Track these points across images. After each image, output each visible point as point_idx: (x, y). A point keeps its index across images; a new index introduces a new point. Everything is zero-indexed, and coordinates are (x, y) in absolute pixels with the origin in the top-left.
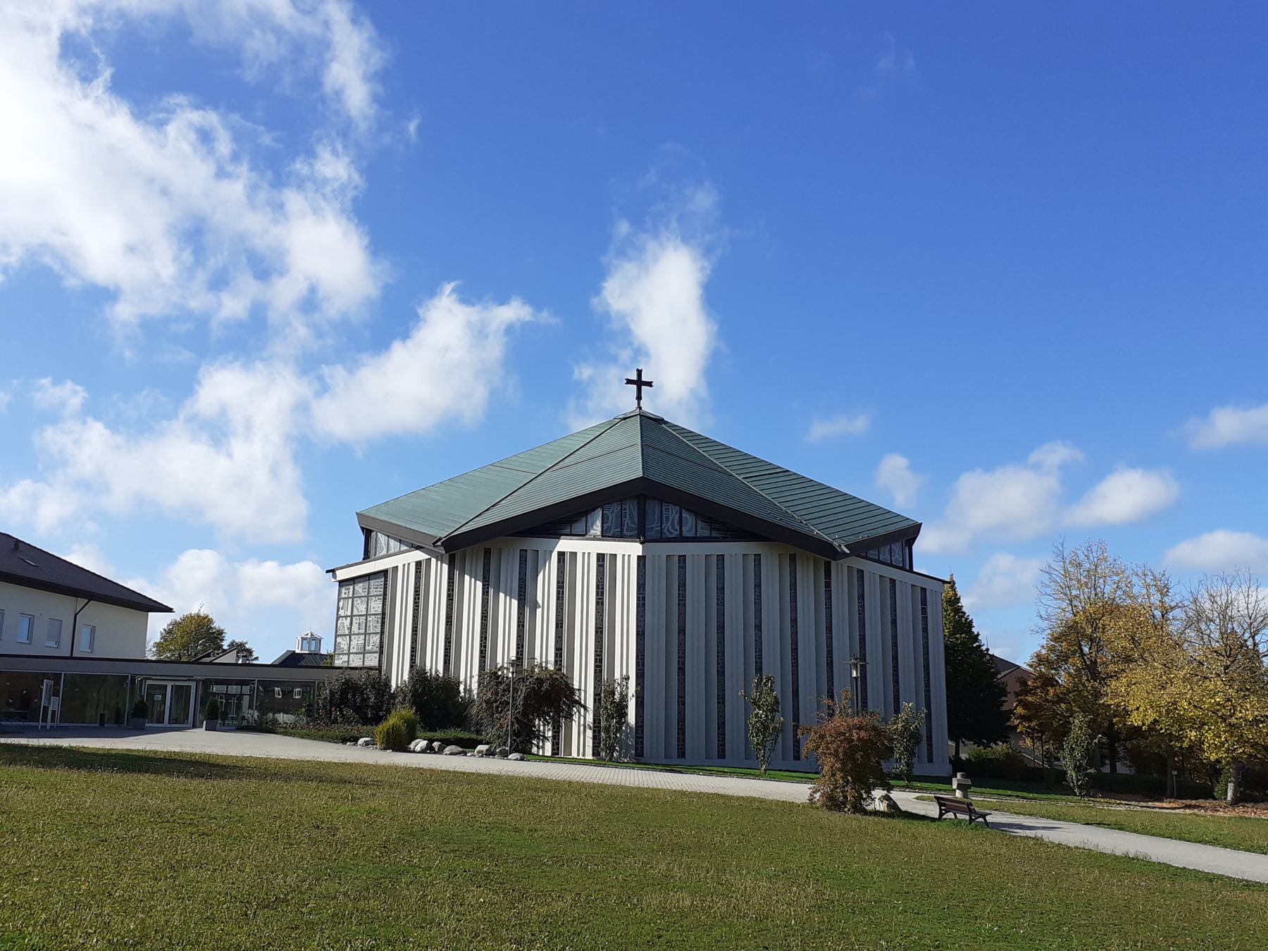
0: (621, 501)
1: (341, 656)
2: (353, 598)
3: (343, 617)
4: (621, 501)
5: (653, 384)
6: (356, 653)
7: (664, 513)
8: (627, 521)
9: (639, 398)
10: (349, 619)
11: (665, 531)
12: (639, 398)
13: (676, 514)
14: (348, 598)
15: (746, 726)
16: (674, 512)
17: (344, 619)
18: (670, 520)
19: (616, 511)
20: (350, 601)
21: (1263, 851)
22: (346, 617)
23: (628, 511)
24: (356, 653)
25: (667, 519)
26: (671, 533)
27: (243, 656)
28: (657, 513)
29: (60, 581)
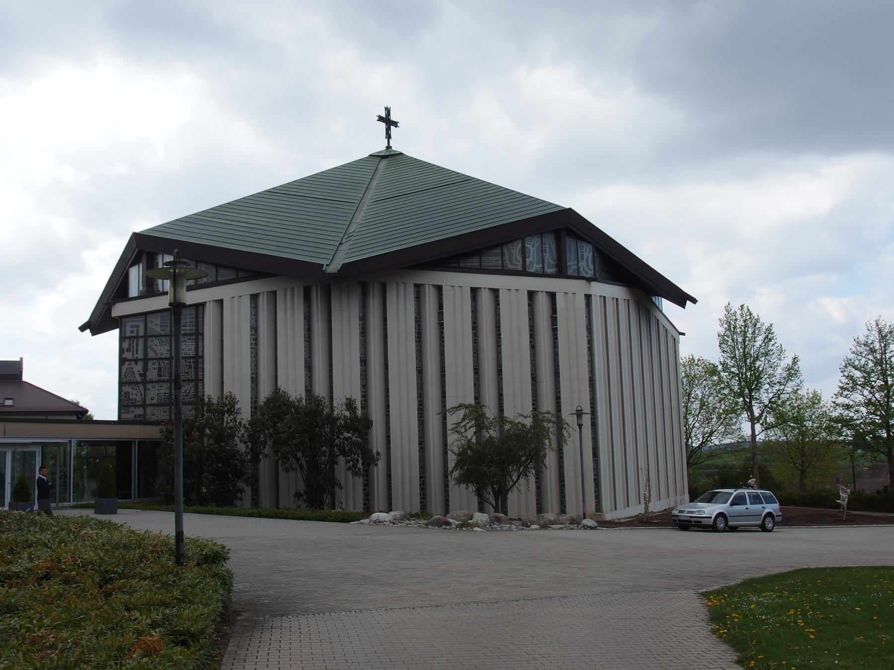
0: (541, 234)
1: (132, 409)
2: (146, 337)
3: (130, 360)
4: (541, 234)
5: (398, 125)
6: (157, 405)
7: (579, 251)
8: (547, 256)
9: (388, 136)
10: (140, 364)
11: (581, 269)
12: (388, 136)
13: (589, 253)
14: (138, 337)
15: (445, 445)
16: (588, 250)
17: (133, 363)
18: (585, 258)
19: (536, 245)
20: (141, 341)
21: (1, 412)
22: (136, 361)
23: (547, 246)
24: (157, 405)
25: (583, 258)
26: (587, 273)
27: (193, 441)
28: (573, 251)
29: (220, 330)
